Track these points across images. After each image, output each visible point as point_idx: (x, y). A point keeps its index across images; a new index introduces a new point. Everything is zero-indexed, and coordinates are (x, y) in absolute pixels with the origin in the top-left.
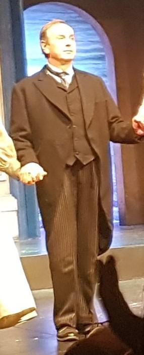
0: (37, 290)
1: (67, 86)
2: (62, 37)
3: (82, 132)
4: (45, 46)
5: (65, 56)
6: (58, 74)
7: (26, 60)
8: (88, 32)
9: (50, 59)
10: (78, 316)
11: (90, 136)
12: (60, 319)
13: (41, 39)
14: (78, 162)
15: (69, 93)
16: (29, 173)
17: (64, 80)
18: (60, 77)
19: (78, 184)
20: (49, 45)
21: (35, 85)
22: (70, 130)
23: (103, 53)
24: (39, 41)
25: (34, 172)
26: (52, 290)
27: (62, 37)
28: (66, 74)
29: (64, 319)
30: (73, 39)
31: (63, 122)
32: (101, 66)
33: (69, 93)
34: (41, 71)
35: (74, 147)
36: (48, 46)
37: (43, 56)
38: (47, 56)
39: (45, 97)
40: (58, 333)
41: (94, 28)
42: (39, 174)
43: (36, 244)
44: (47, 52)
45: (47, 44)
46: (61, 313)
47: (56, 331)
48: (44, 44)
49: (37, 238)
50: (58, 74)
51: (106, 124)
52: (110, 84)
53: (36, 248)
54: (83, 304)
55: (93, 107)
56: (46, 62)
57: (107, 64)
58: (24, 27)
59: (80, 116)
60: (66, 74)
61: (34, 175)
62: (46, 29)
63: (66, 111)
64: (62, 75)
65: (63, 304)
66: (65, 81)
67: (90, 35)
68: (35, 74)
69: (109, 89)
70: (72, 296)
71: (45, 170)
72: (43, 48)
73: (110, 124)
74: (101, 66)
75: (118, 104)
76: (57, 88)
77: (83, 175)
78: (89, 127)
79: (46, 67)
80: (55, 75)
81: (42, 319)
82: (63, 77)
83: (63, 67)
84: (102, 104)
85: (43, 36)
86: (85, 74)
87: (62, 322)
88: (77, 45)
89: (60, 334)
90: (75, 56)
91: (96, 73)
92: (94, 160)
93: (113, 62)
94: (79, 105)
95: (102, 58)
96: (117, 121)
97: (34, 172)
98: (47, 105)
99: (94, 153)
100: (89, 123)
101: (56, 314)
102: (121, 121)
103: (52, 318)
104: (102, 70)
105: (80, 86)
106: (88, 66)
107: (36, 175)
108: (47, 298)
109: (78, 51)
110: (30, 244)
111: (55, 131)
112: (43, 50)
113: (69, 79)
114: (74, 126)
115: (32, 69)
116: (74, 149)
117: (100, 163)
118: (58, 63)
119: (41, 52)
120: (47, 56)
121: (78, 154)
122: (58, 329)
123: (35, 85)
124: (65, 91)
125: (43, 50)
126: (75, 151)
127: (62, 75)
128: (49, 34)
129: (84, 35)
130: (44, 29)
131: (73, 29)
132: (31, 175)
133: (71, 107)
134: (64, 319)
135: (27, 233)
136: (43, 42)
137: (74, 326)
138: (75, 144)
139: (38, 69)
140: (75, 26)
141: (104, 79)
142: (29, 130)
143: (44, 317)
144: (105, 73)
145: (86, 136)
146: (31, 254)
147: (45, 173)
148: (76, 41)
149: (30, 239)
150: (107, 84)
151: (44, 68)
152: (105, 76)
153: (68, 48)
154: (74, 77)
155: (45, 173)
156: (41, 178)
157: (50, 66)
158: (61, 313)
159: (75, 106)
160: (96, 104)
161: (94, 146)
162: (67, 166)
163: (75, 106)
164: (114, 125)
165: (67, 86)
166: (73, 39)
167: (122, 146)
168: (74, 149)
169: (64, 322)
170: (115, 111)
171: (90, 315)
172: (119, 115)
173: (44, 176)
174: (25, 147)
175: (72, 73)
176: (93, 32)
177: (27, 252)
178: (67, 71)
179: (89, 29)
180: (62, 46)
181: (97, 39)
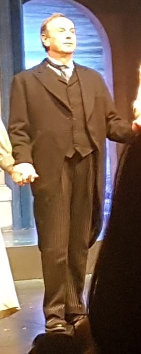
0: (27, 279)
1: (68, 79)
2: (62, 30)
3: (82, 125)
4: (46, 39)
5: (66, 49)
6: (58, 67)
7: (24, 52)
8: (86, 26)
9: (49, 52)
10: (67, 307)
11: (90, 128)
12: (50, 309)
13: (41, 32)
14: (77, 154)
15: (70, 86)
16: (21, 174)
17: (64, 73)
18: (60, 70)
19: (73, 179)
20: (49, 37)
21: (35, 77)
22: (69, 121)
23: (101, 47)
24: (39, 34)
25: (26, 172)
26: (42, 281)
27: (62, 30)
28: (66, 67)
29: (53, 310)
30: (73, 32)
31: (63, 112)
32: (98, 60)
33: (70, 86)
34: (41, 64)
35: (73, 138)
36: (48, 39)
37: (44, 49)
38: (47, 49)
39: (45, 87)
40: (46, 322)
41: (92, 22)
42: (31, 176)
43: (29, 234)
44: (47, 44)
45: (47, 37)
46: (53, 301)
47: (44, 320)
48: (45, 37)
49: (30, 228)
50: (58, 67)
51: (104, 118)
52: (107, 77)
53: (29, 239)
54: (73, 294)
55: (93, 102)
56: (46, 55)
57: (104, 59)
58: (23, 20)
59: (80, 108)
60: (66, 67)
61: (25, 177)
62: (46, 23)
63: (66, 102)
64: (62, 68)
65: (54, 294)
66: (65, 75)
67: (90, 28)
68: (35, 67)
69: (106, 81)
70: (62, 287)
71: (37, 173)
72: (44, 41)
73: (108, 120)
74: (98, 60)
75: (115, 98)
76: (58, 82)
77: (80, 168)
78: (89, 120)
79: (46, 60)
80: (56, 68)
81: (32, 309)
82: (63, 70)
83: (63, 60)
84: (100, 100)
85: (43, 29)
86: (85, 69)
87: (50, 313)
88: (77, 39)
89: (47, 325)
90: (75, 50)
91: (92, 68)
92: (92, 153)
93: (110, 57)
94: (79, 100)
95: (99, 52)
96: (114, 119)
97: (26, 172)
98: (48, 98)
99: (93, 146)
100: (89, 115)
101: (45, 305)
102: (117, 119)
103: (42, 308)
104: (99, 64)
105: (80, 79)
106: (87, 59)
107: (27, 177)
108: (32, 290)
109: (78, 45)
110: (23, 234)
111: (53, 122)
112: (43, 43)
113: (69, 73)
114: (74, 119)
115: (31, 62)
116: (73, 141)
117: (97, 154)
118: (59, 55)
119: (42, 45)
120: (47, 49)
121: (76, 147)
122: (47, 319)
123: (35, 77)
124: (66, 84)
125: (43, 43)
126: (73, 142)
127: (62, 68)
128: (49, 27)
129: (83, 29)
130: (45, 23)
131: (73, 23)
132: (22, 176)
133: (71, 100)
134: (53, 310)
135: (20, 223)
136: (43, 36)
137: (63, 317)
138: (75, 136)
139: (38, 61)
140: (74, 20)
141: (102, 73)
142: (27, 121)
143: (33, 307)
144: (102, 67)
145: (86, 129)
146: (23, 244)
147: (37, 176)
148: (76, 35)
149: (23, 229)
150: (105, 78)
151: (44, 61)
152: (102, 69)
153: (68, 41)
154: (75, 71)
155: (37, 176)
156: (32, 180)
157: (51, 59)
158: (51, 303)
159: (75, 100)
160: (96, 98)
161: (93, 138)
162: (67, 159)
163: (75, 100)
164: (112, 122)
165: (68, 79)
166: (73, 32)
167: (117, 145)
168: (73, 141)
169: (54, 313)
170: (112, 107)
171: (80, 306)
172: (115, 110)
173: (36, 179)
174: (21, 143)
175: (72, 67)
176: (91, 26)
177: (20, 242)
178: (67, 65)
179: (86, 24)
180: (60, 41)
181: (95, 33)
